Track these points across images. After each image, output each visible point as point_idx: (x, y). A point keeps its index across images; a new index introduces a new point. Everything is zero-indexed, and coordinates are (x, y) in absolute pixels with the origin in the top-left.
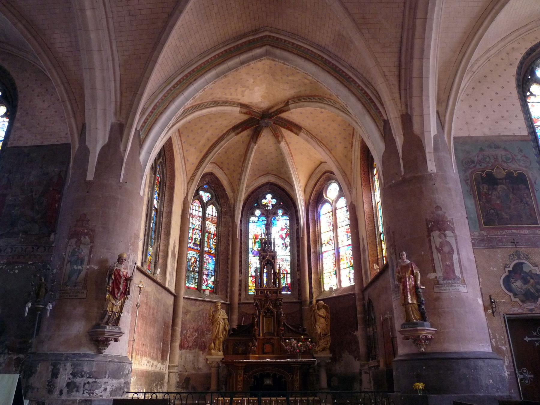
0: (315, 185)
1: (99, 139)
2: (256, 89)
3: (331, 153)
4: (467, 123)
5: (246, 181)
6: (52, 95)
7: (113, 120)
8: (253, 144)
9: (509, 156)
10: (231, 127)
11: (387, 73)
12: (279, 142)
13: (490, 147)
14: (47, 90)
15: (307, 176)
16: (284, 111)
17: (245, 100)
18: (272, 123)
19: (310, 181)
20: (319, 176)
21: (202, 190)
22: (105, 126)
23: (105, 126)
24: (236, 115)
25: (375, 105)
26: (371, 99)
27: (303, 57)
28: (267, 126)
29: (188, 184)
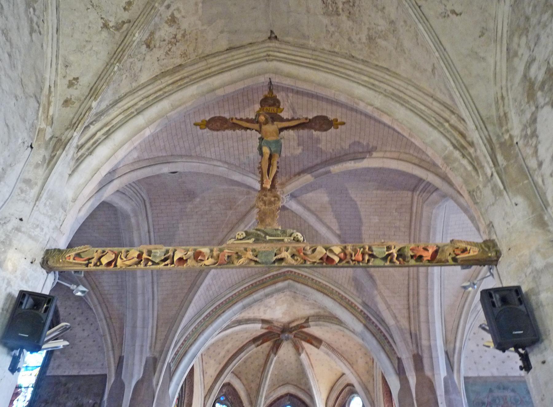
0: (337, 398)
1: (135, 373)
2: (278, 308)
3: (352, 367)
4: (475, 363)
5: (265, 389)
6: (92, 324)
7: (148, 355)
8: (272, 355)
9: (518, 397)
10: (252, 338)
11: (397, 315)
12: (300, 354)
13: (499, 388)
14: (87, 319)
15: (328, 388)
16: (304, 327)
17: (267, 317)
18: (293, 337)
19: (332, 393)
20: (341, 388)
21: (218, 402)
22: (141, 361)
23: (141, 361)
24: (257, 329)
25: (389, 342)
26: (384, 336)
27: (321, 292)
28: (287, 339)
29: (205, 398)
